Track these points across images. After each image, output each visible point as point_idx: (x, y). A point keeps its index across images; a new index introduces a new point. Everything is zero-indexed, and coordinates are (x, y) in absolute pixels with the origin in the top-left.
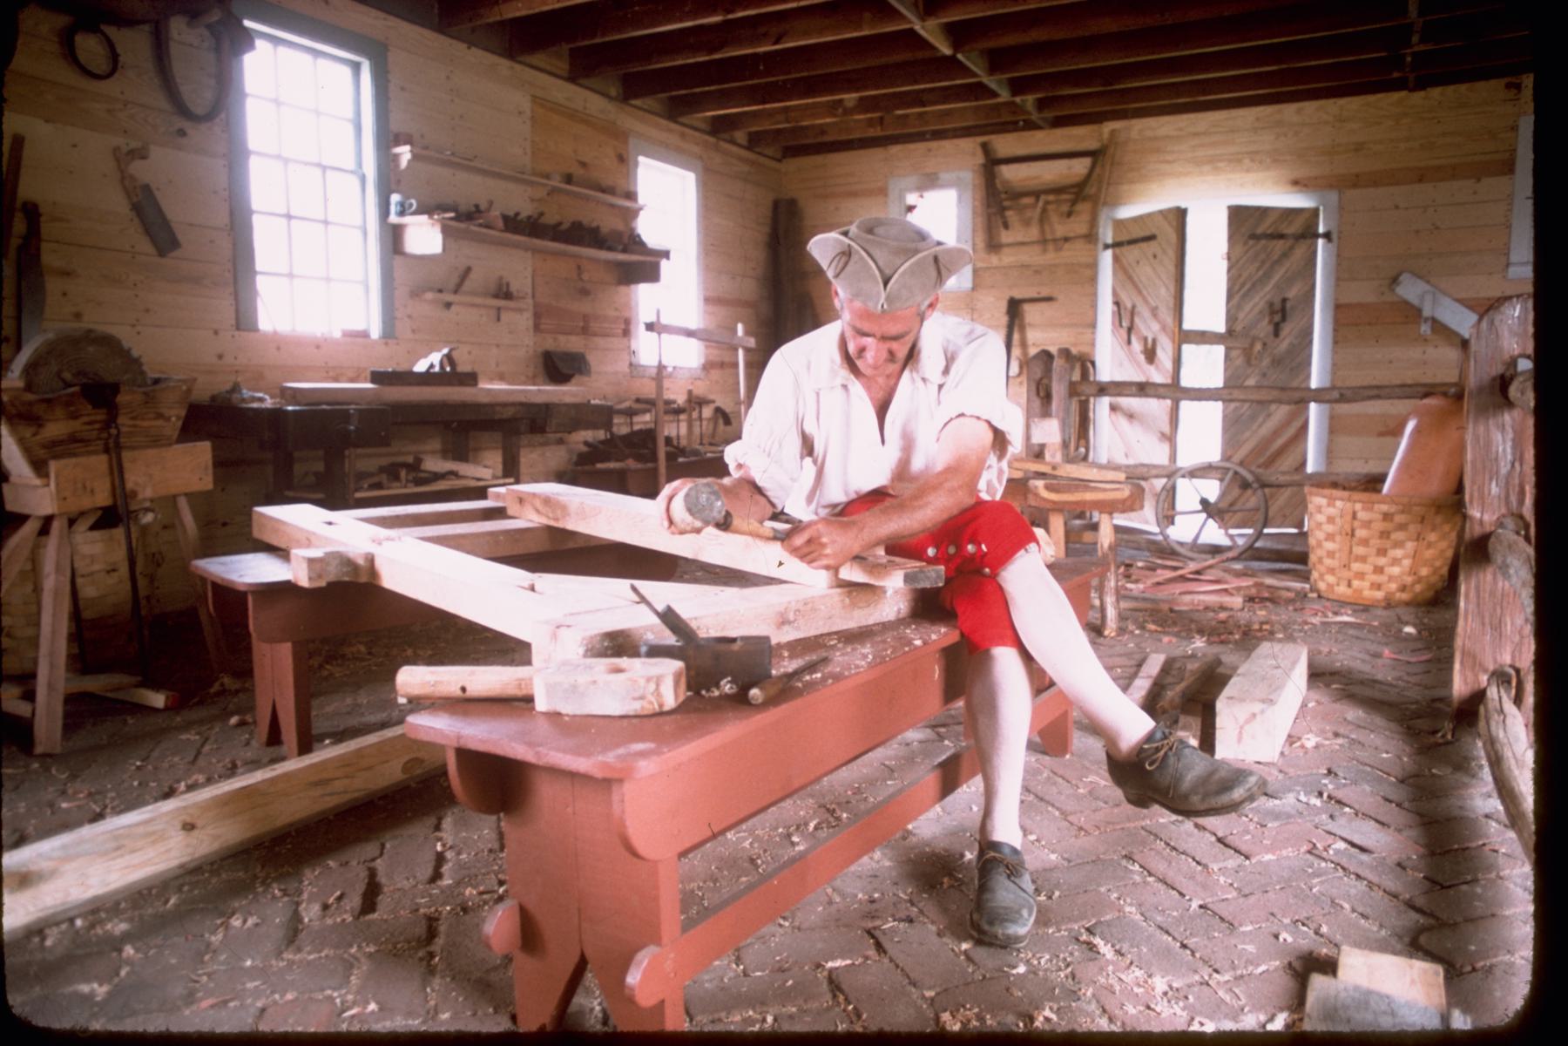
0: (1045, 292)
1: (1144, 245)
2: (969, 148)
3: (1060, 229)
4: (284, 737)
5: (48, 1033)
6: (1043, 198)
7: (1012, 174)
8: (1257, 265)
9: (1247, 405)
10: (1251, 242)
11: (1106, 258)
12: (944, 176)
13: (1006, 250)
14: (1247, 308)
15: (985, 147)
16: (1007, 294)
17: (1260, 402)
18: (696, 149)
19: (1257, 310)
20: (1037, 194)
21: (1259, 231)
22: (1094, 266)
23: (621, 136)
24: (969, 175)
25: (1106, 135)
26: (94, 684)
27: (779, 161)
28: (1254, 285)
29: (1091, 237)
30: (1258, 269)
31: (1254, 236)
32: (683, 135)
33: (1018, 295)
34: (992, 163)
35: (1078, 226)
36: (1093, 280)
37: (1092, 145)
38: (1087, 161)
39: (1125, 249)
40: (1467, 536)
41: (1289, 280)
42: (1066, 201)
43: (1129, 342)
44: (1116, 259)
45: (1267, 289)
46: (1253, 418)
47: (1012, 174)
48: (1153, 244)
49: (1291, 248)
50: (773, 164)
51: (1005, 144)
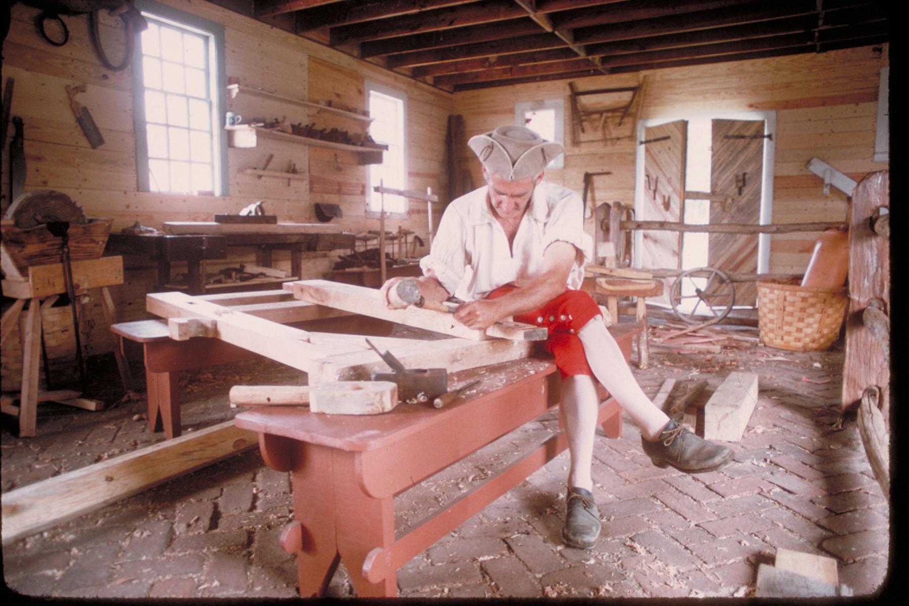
0: (606, 169)
1: (663, 142)
2: (561, 86)
3: (615, 132)
5: (27, 598)
7: (586, 101)
8: (729, 153)
9: (723, 235)
10: (725, 140)
14: (723, 178)
15: (571, 85)
20: (601, 113)
21: (730, 134)
22: (634, 154)
23: (360, 79)
25: (641, 79)
27: (452, 93)
29: (632, 137)
31: (727, 137)
32: (396, 78)
33: (590, 171)
34: (575, 94)
35: (625, 131)
36: (634, 162)
37: (633, 84)
38: (630, 93)
43: (655, 198)
44: (647, 150)
45: (735, 167)
46: (726, 242)
47: (586, 101)
48: (668, 141)
50: (448, 95)
51: (583, 84)
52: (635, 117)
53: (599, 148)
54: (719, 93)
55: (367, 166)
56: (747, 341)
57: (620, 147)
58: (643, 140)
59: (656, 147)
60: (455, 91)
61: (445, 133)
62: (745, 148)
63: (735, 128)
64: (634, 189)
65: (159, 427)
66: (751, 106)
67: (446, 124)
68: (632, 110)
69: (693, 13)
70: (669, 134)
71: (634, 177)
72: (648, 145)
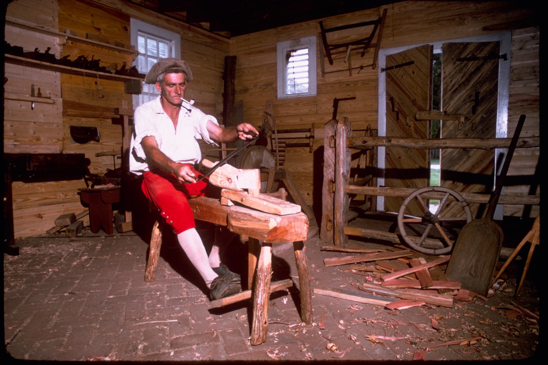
2: (314, 23)
5: (16, 359)
6: (350, 47)
7: (333, 37)
8: (461, 75)
9: (457, 151)
12: (303, 40)
13: (364, 68)
14: (456, 99)
15: (321, 23)
18: (177, 29)
19: (463, 98)
20: (346, 45)
22: (377, 80)
23: (126, 18)
24: (314, 39)
28: (460, 86)
29: (374, 65)
30: (462, 77)
31: (459, 59)
32: (168, 21)
34: (324, 32)
35: (367, 61)
36: (376, 88)
37: (375, 18)
38: (372, 27)
39: (395, 71)
43: (398, 119)
45: (468, 88)
46: (460, 158)
47: (333, 37)
49: (483, 65)
51: (331, 22)
52: (377, 47)
53: (344, 77)
56: (439, 291)
57: (366, 74)
58: (384, 67)
59: (397, 73)
61: (222, 70)
63: (468, 51)
64: (377, 111)
65: (405, 218)
72: (389, 71)
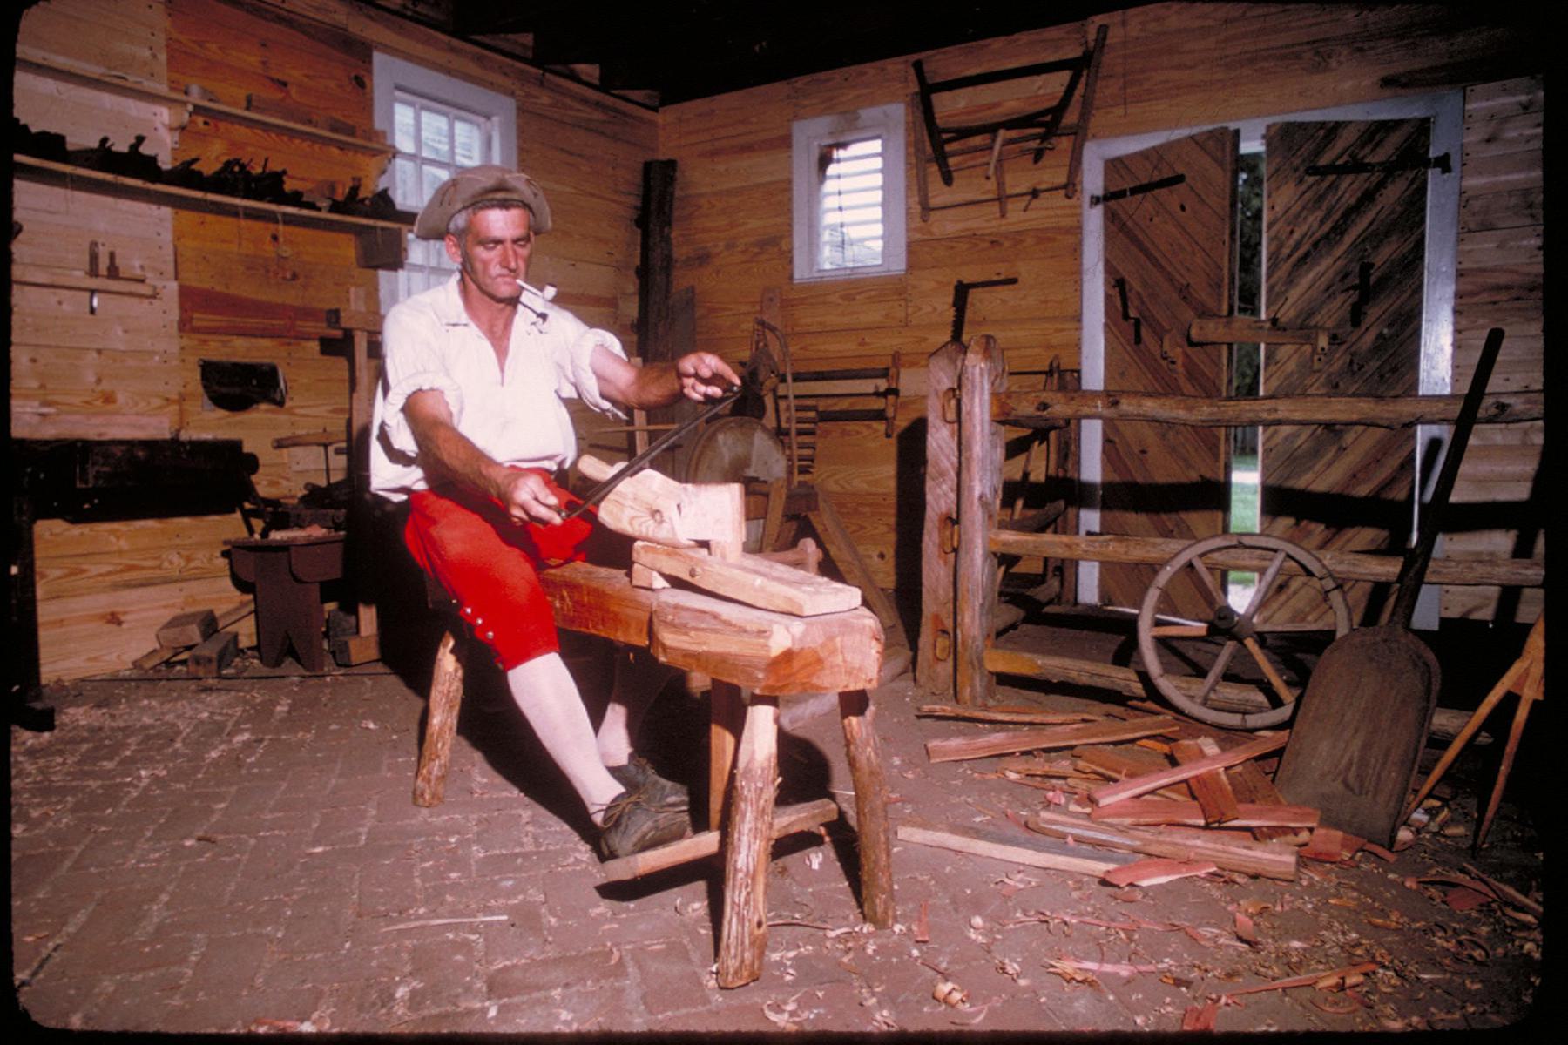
0: (1004, 271)
1: (1162, 193)
2: (898, 67)
3: (1019, 181)
4: (801, 384)
6: (1003, 134)
8: (1320, 214)
9: (1307, 432)
10: (1310, 179)
11: (1094, 220)
12: (867, 114)
14: (1305, 281)
15: (918, 67)
16: (952, 277)
17: (1329, 426)
20: (991, 129)
21: (1324, 161)
22: (1077, 230)
23: (361, 52)
24: (898, 112)
25: (1092, 36)
26: (652, 427)
27: (655, 110)
28: (1315, 245)
29: (1070, 187)
30: (1322, 222)
31: (1313, 170)
32: (480, 60)
33: (968, 276)
34: (926, 92)
35: (1051, 173)
36: (1076, 251)
37: (1073, 52)
38: (1065, 76)
39: (1130, 203)
40: (597, 82)
41: (1376, 237)
42: (1033, 137)
43: (1138, 339)
44: (1111, 218)
46: (1315, 453)
47: (951, 107)
48: (1180, 187)
49: (1381, 184)
50: (648, 114)
51: (945, 62)
54: (1298, 56)
55: (1539, 314)
58: (1099, 192)
60: (663, 104)
62: (1368, 197)
63: (1340, 144)
64: (1078, 319)
66: (1387, 82)
67: (639, 179)
68: (1071, 118)
69: (263, 337)
70: (1180, 170)
71: (1078, 283)
72: (1112, 203)
